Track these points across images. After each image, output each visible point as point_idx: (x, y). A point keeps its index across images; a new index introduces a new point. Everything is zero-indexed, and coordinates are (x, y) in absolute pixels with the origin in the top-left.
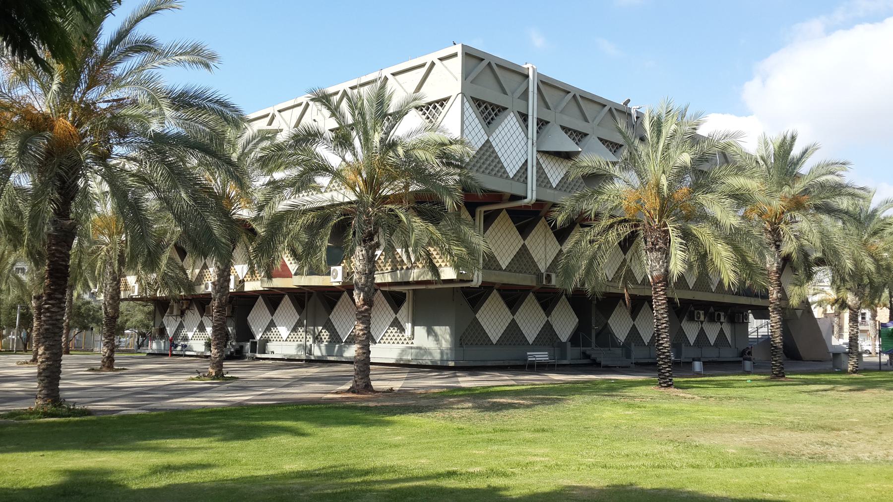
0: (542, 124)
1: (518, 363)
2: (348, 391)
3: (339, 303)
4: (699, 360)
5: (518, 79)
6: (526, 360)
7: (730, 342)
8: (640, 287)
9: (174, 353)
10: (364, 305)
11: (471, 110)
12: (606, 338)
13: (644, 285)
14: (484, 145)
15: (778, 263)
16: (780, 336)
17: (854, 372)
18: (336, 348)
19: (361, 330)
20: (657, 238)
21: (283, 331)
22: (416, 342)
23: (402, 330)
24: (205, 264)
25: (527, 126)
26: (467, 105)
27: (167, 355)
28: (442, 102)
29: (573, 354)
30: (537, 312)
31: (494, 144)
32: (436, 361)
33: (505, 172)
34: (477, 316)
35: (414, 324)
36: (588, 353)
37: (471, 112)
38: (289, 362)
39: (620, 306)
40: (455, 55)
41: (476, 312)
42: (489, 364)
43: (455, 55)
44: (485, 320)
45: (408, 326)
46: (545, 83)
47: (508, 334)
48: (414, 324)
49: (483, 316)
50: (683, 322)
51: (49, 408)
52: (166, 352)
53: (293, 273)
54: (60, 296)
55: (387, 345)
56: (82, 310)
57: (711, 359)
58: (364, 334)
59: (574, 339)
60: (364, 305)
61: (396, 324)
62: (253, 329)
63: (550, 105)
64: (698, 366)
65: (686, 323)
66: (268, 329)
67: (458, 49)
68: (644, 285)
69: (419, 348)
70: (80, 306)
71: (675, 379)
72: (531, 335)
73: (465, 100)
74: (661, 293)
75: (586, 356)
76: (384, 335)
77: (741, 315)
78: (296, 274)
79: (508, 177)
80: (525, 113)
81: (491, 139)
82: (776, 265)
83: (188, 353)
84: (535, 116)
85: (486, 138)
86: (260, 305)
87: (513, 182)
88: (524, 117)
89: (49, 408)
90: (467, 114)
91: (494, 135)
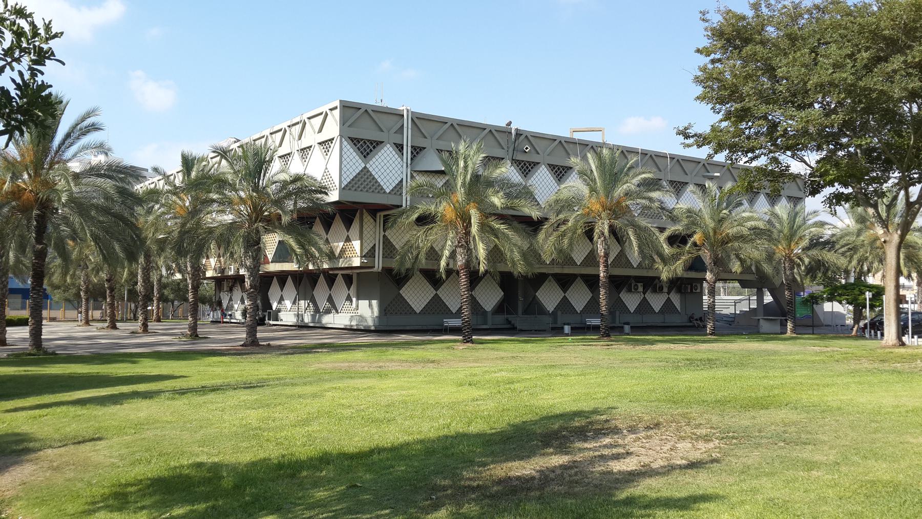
0: (417, 151)
1: (437, 327)
2: (242, 346)
3: (337, 279)
4: (568, 324)
5: (395, 118)
6: (443, 325)
7: (679, 309)
8: (550, 266)
9: (225, 320)
10: (251, 289)
11: (348, 147)
12: (535, 308)
13: (553, 264)
14: (362, 171)
15: (605, 249)
16: (606, 305)
17: (711, 334)
18: (317, 317)
19: (249, 305)
20: (460, 238)
21: (288, 303)
22: (360, 312)
23: (351, 301)
24: (348, 236)
25: (403, 154)
26: (345, 143)
27: (220, 322)
28: (331, 140)
29: (500, 319)
30: (427, 289)
31: (371, 169)
32: (370, 327)
33: (382, 189)
34: (401, 292)
35: (358, 299)
36: (510, 319)
37: (347, 146)
38: (287, 327)
39: (550, 281)
40: (336, 108)
41: (400, 289)
42: (408, 328)
43: (336, 108)
44: (409, 295)
45: (354, 300)
46: (419, 120)
47: (433, 303)
48: (358, 299)
49: (406, 292)
50: (647, 293)
51: (35, 351)
52: (219, 320)
53: (270, 261)
54: (39, 288)
55: (344, 314)
56: (181, 286)
57: (649, 324)
58: (251, 308)
59: (500, 308)
60: (251, 289)
61: (349, 299)
62: (271, 301)
63: (426, 134)
64: (627, 328)
65: (625, 293)
66: (280, 302)
67: (337, 104)
68: (553, 264)
69: (360, 316)
70: (179, 283)
71: (474, 337)
72: (454, 306)
73: (343, 140)
74: (464, 277)
75: (509, 322)
76: (343, 307)
77: (689, 286)
78: (272, 262)
79: (385, 192)
80: (401, 143)
81: (368, 166)
82: (603, 251)
83: (232, 321)
84: (409, 145)
85: (363, 165)
86: (322, 281)
87: (390, 195)
88: (399, 147)
89: (35, 351)
90: (345, 150)
91: (371, 162)
